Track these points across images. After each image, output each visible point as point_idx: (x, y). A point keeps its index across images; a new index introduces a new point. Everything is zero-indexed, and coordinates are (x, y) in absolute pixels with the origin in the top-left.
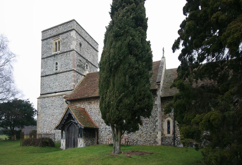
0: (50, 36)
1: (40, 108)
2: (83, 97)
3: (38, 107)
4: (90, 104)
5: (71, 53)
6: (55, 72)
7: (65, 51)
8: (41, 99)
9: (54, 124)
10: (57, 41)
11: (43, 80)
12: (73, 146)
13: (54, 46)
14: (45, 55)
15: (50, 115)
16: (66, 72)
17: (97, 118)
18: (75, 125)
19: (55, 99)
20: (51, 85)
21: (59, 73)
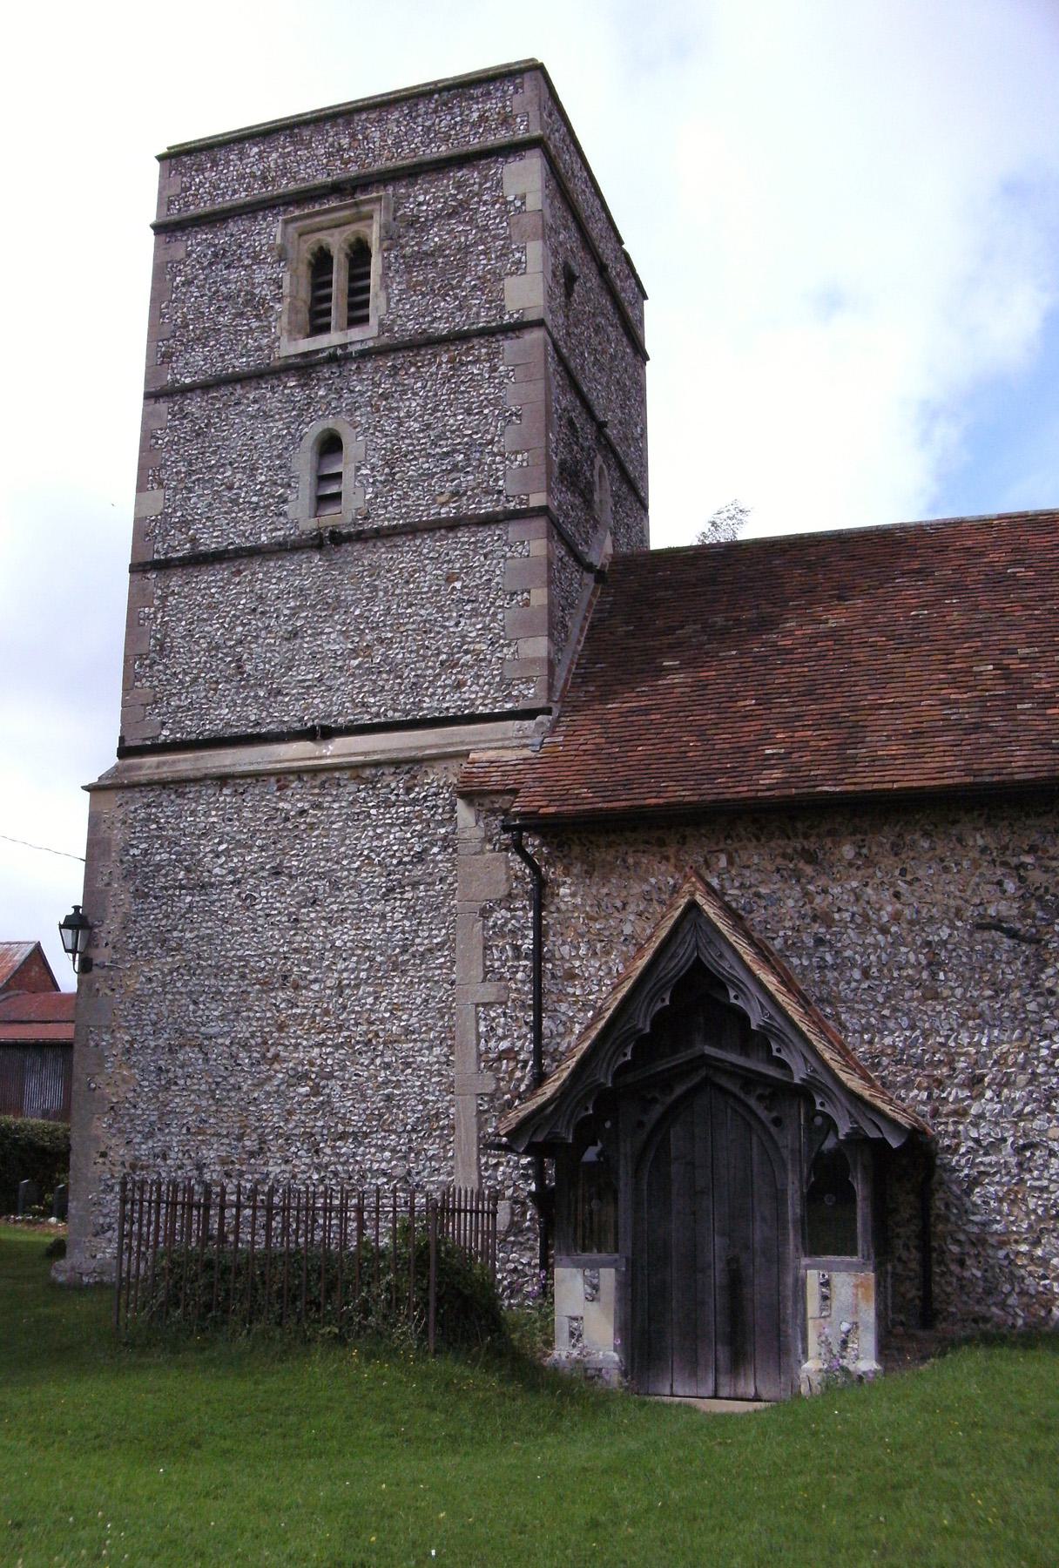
0: (259, 192)
1: (121, 896)
2: (743, 790)
3: (100, 885)
4: (809, 870)
5: (508, 345)
6: (309, 524)
7: (442, 328)
8: (138, 799)
9: (306, 1076)
10: (337, 242)
11: (163, 598)
12: (723, 1354)
13: (294, 282)
14: (196, 364)
15: (243, 976)
16: (453, 525)
17: (913, 1028)
18: (752, 1102)
19: (318, 806)
20: (263, 655)
21: (366, 540)
